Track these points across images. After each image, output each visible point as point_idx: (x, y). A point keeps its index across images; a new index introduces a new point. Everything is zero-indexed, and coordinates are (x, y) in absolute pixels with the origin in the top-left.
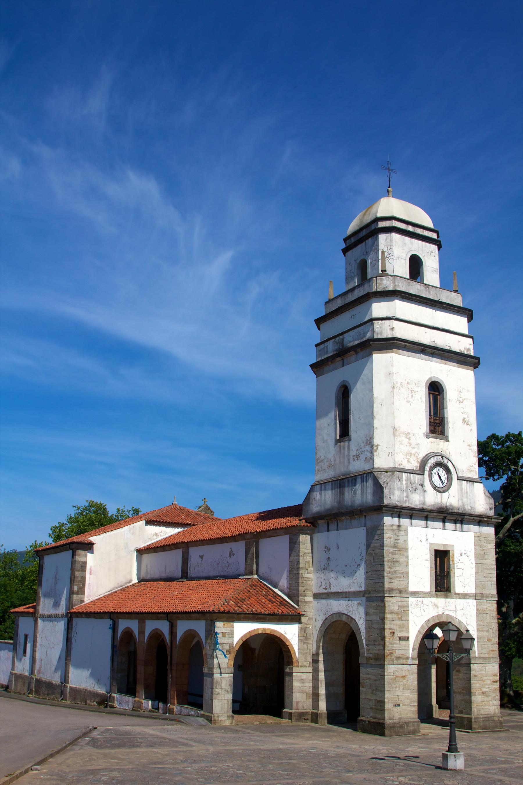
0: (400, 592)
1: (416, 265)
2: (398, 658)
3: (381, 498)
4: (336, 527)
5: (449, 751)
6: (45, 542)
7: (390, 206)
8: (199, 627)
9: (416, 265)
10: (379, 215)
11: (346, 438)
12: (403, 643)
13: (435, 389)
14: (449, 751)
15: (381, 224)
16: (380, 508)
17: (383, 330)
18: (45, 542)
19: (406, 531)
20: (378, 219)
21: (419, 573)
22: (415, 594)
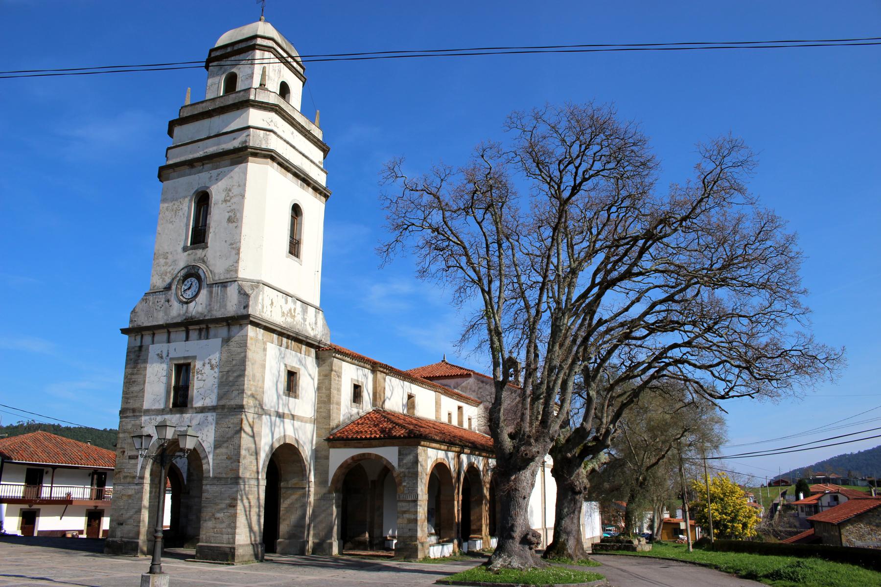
0: (134, 410)
1: (284, 90)
2: (125, 477)
3: (246, 307)
4: (184, 335)
5: (150, 572)
6: (790, 239)
7: (264, 28)
8: (390, 454)
9: (284, 90)
10: (259, 33)
11: (200, 242)
12: (133, 461)
13: (296, 210)
14: (150, 572)
15: (259, 41)
16: (242, 319)
17: (257, 140)
18: (790, 239)
19: (148, 349)
20: (256, 37)
21: (347, 393)
22: (147, 412)
